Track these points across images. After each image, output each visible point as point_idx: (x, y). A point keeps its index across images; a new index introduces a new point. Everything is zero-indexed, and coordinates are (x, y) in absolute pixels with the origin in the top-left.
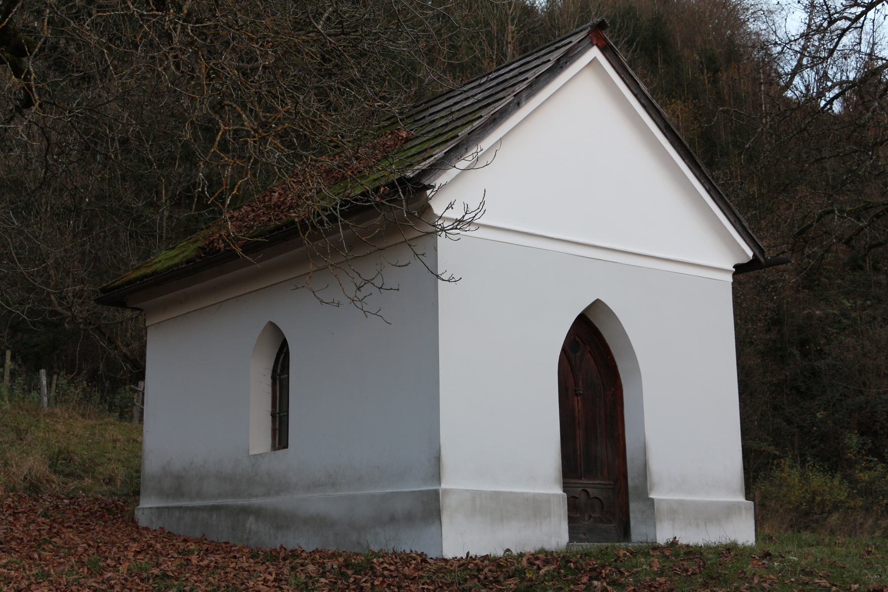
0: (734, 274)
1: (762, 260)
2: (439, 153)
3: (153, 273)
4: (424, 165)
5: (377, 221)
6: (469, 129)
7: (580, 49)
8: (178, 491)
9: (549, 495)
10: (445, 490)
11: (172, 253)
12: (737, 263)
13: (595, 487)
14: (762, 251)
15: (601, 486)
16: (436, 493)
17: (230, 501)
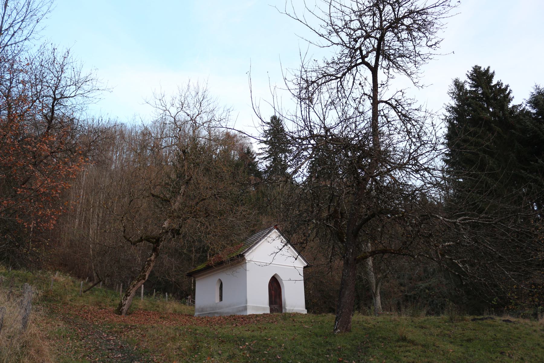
2: (247, 250)
5: (235, 261)
13: (276, 307)
17: (212, 312)
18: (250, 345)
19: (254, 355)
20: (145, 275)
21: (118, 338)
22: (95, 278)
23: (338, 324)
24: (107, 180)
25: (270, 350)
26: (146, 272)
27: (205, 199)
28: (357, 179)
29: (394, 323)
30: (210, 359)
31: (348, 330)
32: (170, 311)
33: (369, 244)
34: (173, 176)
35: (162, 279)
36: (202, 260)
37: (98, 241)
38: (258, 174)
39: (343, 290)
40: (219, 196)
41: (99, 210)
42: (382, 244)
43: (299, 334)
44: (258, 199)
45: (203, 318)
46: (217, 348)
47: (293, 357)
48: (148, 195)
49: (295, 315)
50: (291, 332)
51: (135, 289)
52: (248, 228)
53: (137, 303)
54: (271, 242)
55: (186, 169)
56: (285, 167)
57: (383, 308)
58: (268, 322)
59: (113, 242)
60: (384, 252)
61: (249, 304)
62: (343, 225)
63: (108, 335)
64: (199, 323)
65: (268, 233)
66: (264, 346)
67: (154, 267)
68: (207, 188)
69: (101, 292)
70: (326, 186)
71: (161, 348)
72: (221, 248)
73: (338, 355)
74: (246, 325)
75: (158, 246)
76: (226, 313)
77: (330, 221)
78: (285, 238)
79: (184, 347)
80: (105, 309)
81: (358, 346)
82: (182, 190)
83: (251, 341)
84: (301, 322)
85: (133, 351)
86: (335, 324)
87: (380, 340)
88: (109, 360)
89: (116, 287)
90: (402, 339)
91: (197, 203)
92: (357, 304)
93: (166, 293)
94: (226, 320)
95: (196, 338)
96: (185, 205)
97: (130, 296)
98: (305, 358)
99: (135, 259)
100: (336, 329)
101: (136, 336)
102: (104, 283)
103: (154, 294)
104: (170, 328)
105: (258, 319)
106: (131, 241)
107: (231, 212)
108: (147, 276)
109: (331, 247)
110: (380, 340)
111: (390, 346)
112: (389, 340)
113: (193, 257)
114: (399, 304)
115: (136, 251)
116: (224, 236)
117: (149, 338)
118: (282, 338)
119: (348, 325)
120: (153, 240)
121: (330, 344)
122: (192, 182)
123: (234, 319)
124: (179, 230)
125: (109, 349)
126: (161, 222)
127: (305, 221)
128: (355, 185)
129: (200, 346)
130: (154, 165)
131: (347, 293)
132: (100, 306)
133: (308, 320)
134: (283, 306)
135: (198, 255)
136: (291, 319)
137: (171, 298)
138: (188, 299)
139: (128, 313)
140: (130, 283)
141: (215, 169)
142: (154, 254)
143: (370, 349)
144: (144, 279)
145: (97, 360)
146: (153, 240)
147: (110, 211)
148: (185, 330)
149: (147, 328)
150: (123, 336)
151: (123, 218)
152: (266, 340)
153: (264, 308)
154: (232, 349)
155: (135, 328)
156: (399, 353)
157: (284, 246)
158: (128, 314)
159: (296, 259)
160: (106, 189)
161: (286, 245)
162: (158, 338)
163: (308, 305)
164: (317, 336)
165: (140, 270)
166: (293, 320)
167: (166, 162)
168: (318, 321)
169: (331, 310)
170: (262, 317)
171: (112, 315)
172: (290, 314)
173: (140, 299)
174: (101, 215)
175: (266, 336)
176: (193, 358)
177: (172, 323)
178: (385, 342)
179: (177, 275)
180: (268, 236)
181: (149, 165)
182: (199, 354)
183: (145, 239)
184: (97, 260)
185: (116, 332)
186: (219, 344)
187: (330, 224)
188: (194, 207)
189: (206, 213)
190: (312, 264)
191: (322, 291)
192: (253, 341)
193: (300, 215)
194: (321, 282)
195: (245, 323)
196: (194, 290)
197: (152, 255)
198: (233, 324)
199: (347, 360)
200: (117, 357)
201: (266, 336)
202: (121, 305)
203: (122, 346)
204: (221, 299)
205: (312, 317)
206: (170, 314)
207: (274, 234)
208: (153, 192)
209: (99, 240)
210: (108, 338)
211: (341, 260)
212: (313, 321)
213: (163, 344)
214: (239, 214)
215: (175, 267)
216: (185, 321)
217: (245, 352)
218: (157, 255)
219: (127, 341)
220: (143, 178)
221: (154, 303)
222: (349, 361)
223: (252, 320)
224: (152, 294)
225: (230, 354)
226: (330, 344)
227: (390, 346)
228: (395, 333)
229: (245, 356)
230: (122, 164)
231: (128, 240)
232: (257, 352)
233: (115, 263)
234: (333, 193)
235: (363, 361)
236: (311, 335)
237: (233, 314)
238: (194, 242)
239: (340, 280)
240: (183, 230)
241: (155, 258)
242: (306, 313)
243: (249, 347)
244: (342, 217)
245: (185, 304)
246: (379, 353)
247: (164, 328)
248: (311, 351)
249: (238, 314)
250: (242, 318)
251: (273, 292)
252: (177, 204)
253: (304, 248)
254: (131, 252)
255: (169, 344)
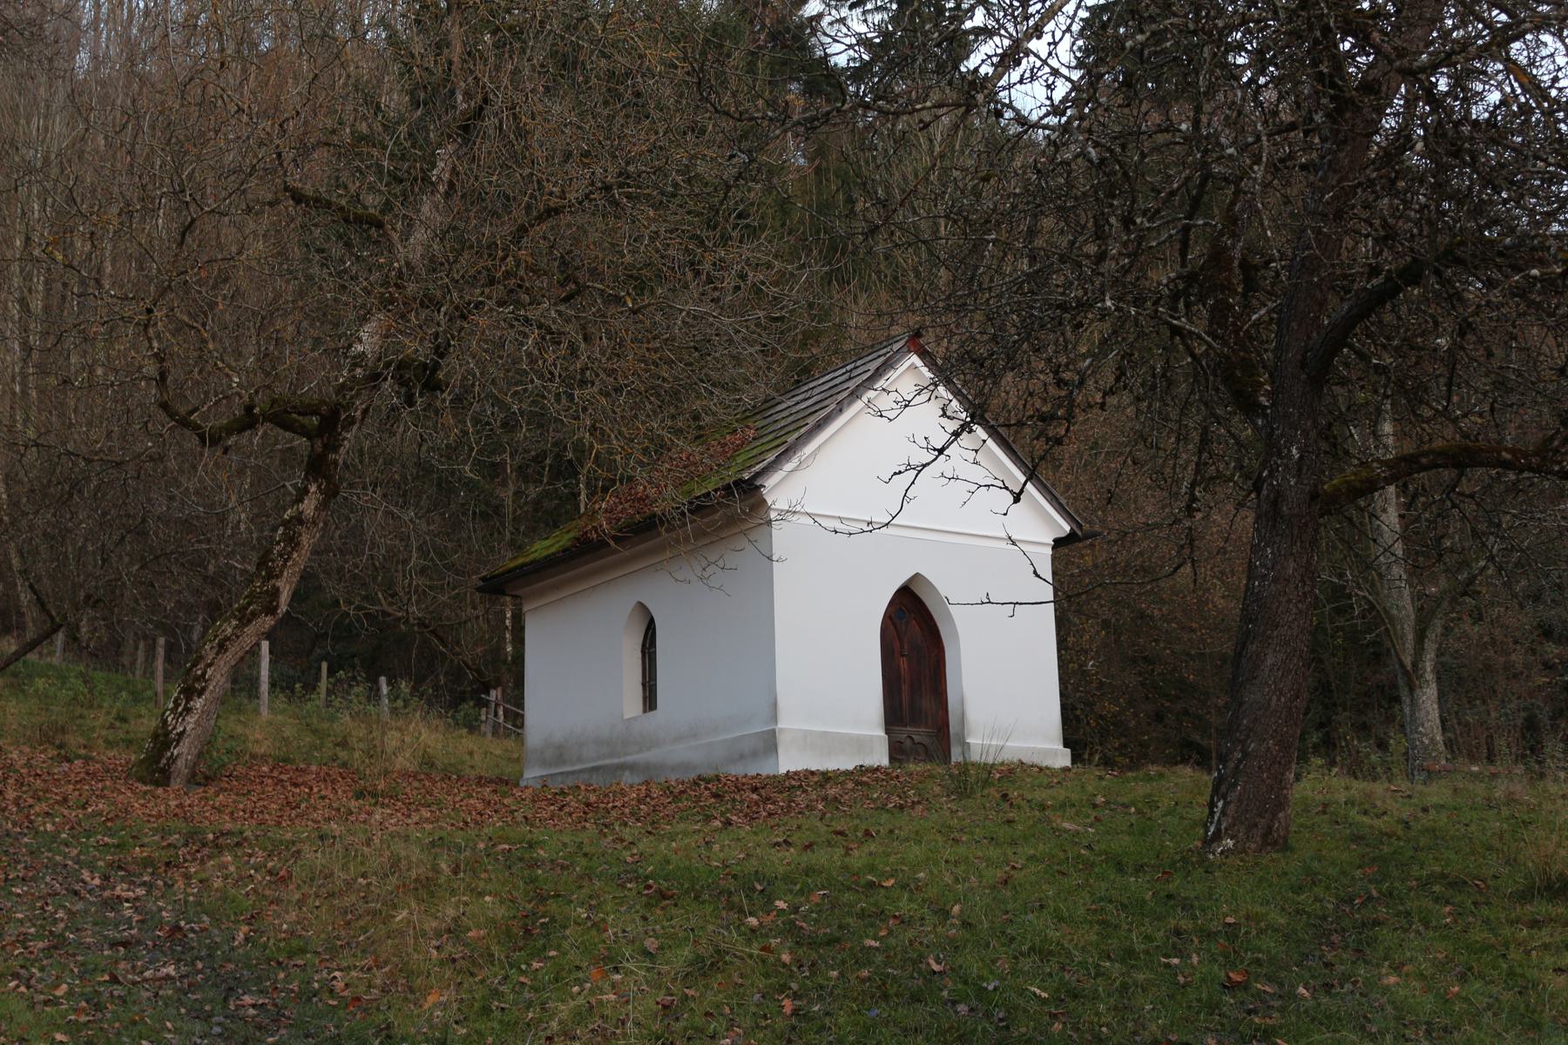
0: (1054, 548)
1: (1079, 533)
2: (771, 457)
3: (532, 562)
4: (758, 468)
5: (716, 516)
6: (796, 435)
8: (560, 759)
10: (781, 729)
11: (547, 543)
13: (920, 734)
14: (1080, 526)
16: (774, 731)
17: (607, 762)
18: (795, 909)
19: (815, 956)
20: (276, 593)
21: (156, 893)
22: (28, 619)
23: (1223, 812)
24: (58, 125)
25: (890, 933)
26: (278, 577)
27: (557, 211)
28: (1333, 85)
29: (1505, 812)
30: (605, 975)
31: (1275, 841)
32: (403, 762)
33: (1387, 428)
34: (394, 100)
35: (359, 608)
36: (549, 516)
37: (31, 434)
38: (823, 78)
39: (1253, 648)
40: (629, 196)
41: (28, 278)
42: (1455, 421)
43: (1031, 858)
44: (825, 207)
45: (563, 793)
46: (635, 928)
47: (1004, 965)
48: (270, 197)
49: (1011, 771)
50: (993, 852)
51: (230, 657)
52: (775, 351)
53: (240, 729)
54: (891, 415)
55: (456, 59)
56: (961, 44)
57: (1449, 744)
58: (883, 808)
59: (109, 435)
60: (1463, 458)
61: (789, 722)
62: (1257, 324)
63: (106, 878)
64: (544, 814)
65: (878, 373)
66: (862, 915)
67: (315, 552)
68: (568, 156)
69: (64, 679)
70: (1170, 128)
71: (364, 930)
72: (645, 451)
73: (1226, 957)
74: (771, 822)
75: (336, 449)
76: (673, 768)
77: (1188, 306)
78: (957, 393)
79: (479, 927)
80: (87, 759)
81: (1324, 918)
82: (441, 171)
83: (801, 892)
84: (1043, 807)
85: (233, 949)
86: (1212, 813)
87: (1437, 888)
88: (118, 991)
89: (134, 655)
90: (1549, 888)
91: (523, 230)
92: (1321, 725)
93: (383, 680)
94: (677, 798)
95: (533, 880)
96: (462, 241)
97: (207, 694)
98: (1063, 969)
99: (222, 518)
100: (1218, 836)
101: (242, 880)
102: (75, 639)
103: (323, 685)
104: (407, 838)
105: (832, 791)
106: (196, 427)
107: (690, 275)
108: (284, 598)
109: (1195, 436)
110: (1437, 888)
111: (1486, 921)
112: (1480, 892)
113: (509, 502)
114: (1531, 725)
115: (222, 476)
116: (658, 395)
117: (305, 889)
118: (948, 879)
119: (1274, 815)
120: (305, 420)
121: (1187, 906)
122: (490, 122)
123: (715, 796)
124: (436, 367)
125: (114, 945)
126: (342, 330)
127: (1063, 307)
128: (1318, 118)
129: (553, 920)
130: (293, 44)
131: (1269, 662)
132: (60, 747)
133: (1074, 797)
134: (953, 728)
135: (533, 491)
136: (992, 791)
137: (406, 703)
138: (486, 704)
139: (199, 778)
140: (203, 635)
141: (604, 55)
142: (313, 488)
143: (1383, 933)
144: (271, 610)
145: (59, 993)
146: (305, 420)
147: (83, 282)
148: (482, 846)
149: (293, 843)
150: (180, 884)
151: (149, 311)
152: (871, 885)
153: (860, 743)
154: (711, 928)
155: (238, 844)
156: (1528, 953)
157: (956, 434)
158: (201, 778)
159: (1017, 499)
160: (54, 172)
161: (965, 427)
162: (349, 884)
163: (1074, 731)
164: (1120, 867)
165: (251, 568)
166: (1005, 796)
167: (356, 23)
168: (1125, 800)
169: (1192, 753)
170: (850, 785)
171: (120, 785)
172: (988, 769)
173: (257, 712)
174: (37, 305)
175: (872, 869)
176: (522, 972)
177: (415, 817)
178: (1458, 899)
179: (430, 588)
180: (881, 383)
181: (265, 45)
182: (553, 953)
183: (267, 418)
184: (31, 528)
185: (147, 863)
186: (648, 906)
187: (1190, 321)
188: (506, 249)
189: (567, 279)
190: (1097, 528)
191: (1145, 659)
192: (811, 891)
193: (1038, 278)
194: (1142, 615)
195: (770, 815)
196: (519, 659)
197: (306, 491)
198: (708, 819)
199: (1270, 979)
200: (155, 979)
201: (872, 869)
202: (163, 740)
203: (179, 928)
204: (650, 701)
205: (1097, 781)
206: (406, 775)
207: (909, 373)
208: (294, 181)
209: (37, 428)
210: (107, 894)
211: (1240, 505)
212: (1100, 799)
213: (374, 913)
214: (729, 282)
215: (423, 553)
216: (480, 806)
217: (774, 942)
218: (330, 493)
219: (199, 904)
220: (240, 110)
221: (326, 725)
222: (1281, 985)
223: (800, 798)
224: (311, 687)
225: (701, 951)
226: (1187, 906)
227: (1486, 921)
228: (1512, 862)
229: (772, 959)
230: (129, 45)
231: (184, 423)
232: (832, 941)
233: (123, 538)
234: (1204, 165)
235: (1348, 987)
236: (1093, 865)
237: (711, 773)
238: (509, 425)
239: (1235, 607)
240: (453, 368)
241: (323, 506)
242: (1067, 762)
243: (792, 922)
244: (1250, 285)
245: (472, 728)
246: (1426, 950)
247: (377, 841)
248: (1094, 938)
249: (737, 770)
250: (755, 790)
251: (903, 664)
252: (420, 235)
253: (1059, 441)
254: (201, 480)
255: (405, 913)
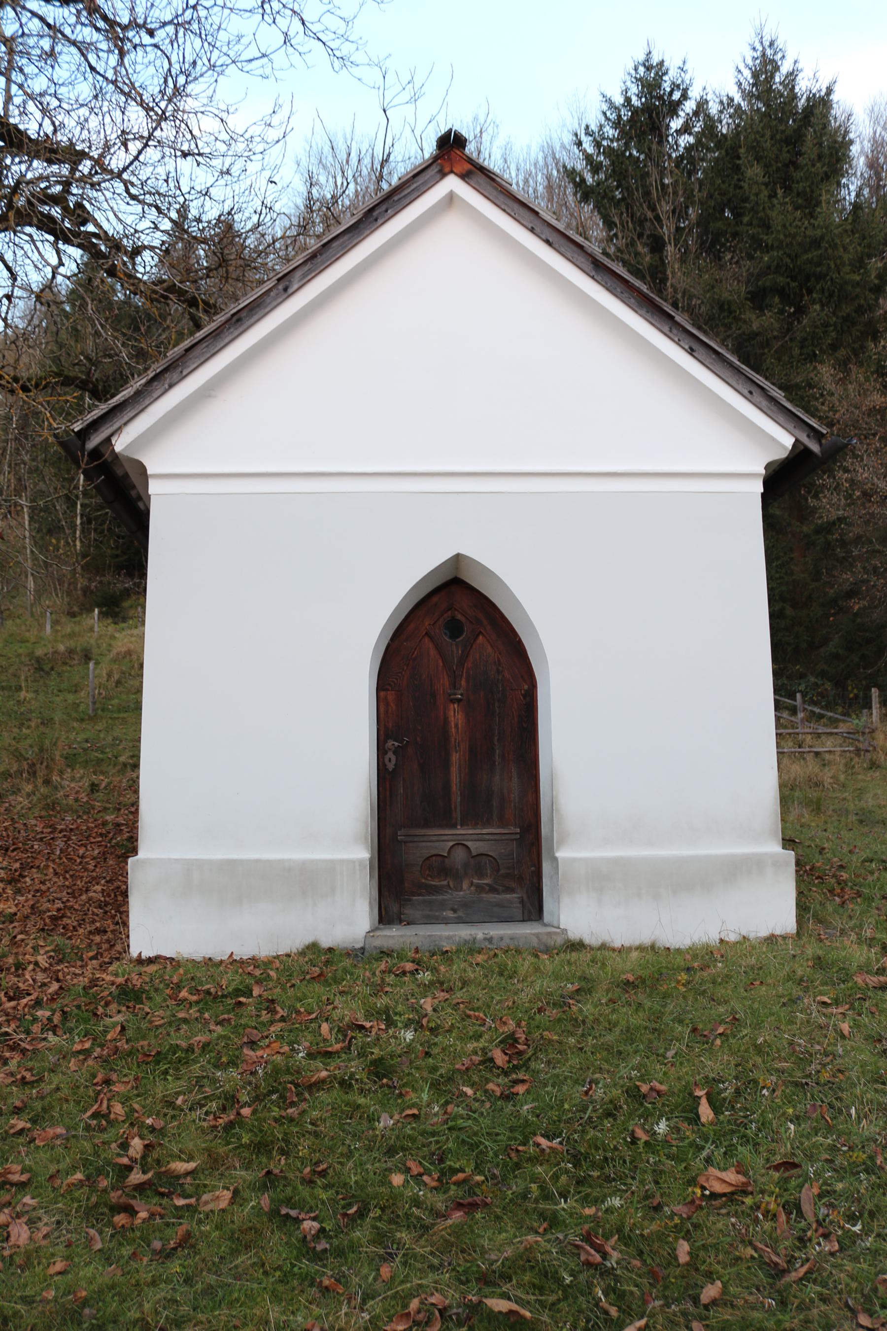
7: (415, 185)
9: (333, 861)
12: (770, 459)
15: (495, 837)
